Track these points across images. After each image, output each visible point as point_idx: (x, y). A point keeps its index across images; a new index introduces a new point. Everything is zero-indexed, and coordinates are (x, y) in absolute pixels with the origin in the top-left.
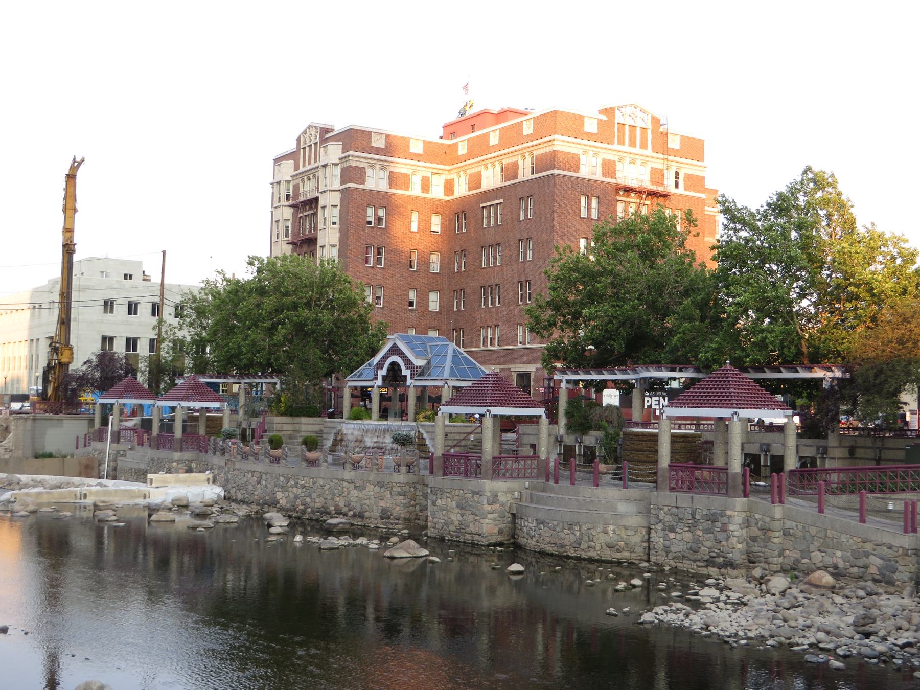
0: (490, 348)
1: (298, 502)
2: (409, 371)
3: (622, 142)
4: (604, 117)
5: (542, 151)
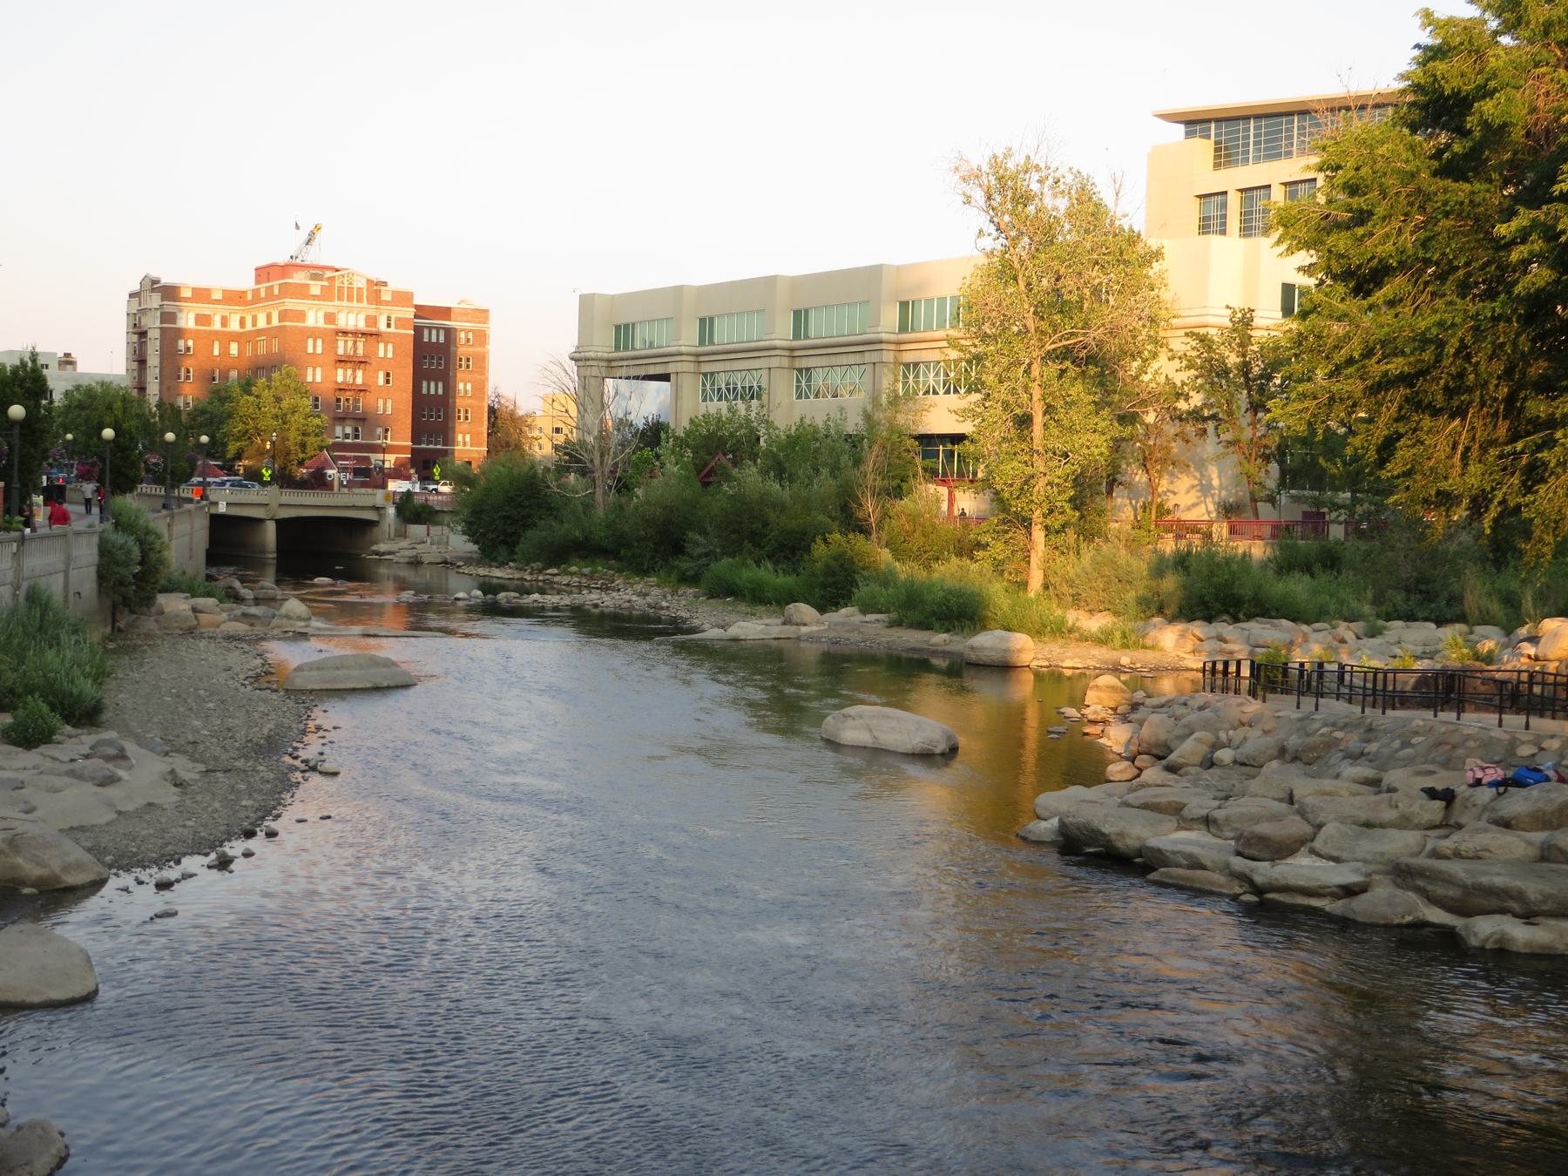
3: (341, 299)
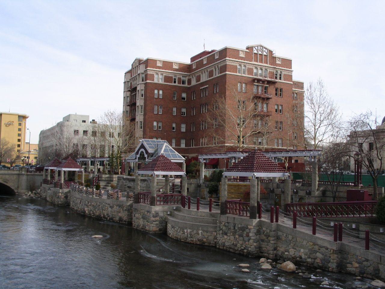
0: (204, 146)
1: (91, 212)
2: (147, 155)
4: (247, 51)
5: (222, 65)
